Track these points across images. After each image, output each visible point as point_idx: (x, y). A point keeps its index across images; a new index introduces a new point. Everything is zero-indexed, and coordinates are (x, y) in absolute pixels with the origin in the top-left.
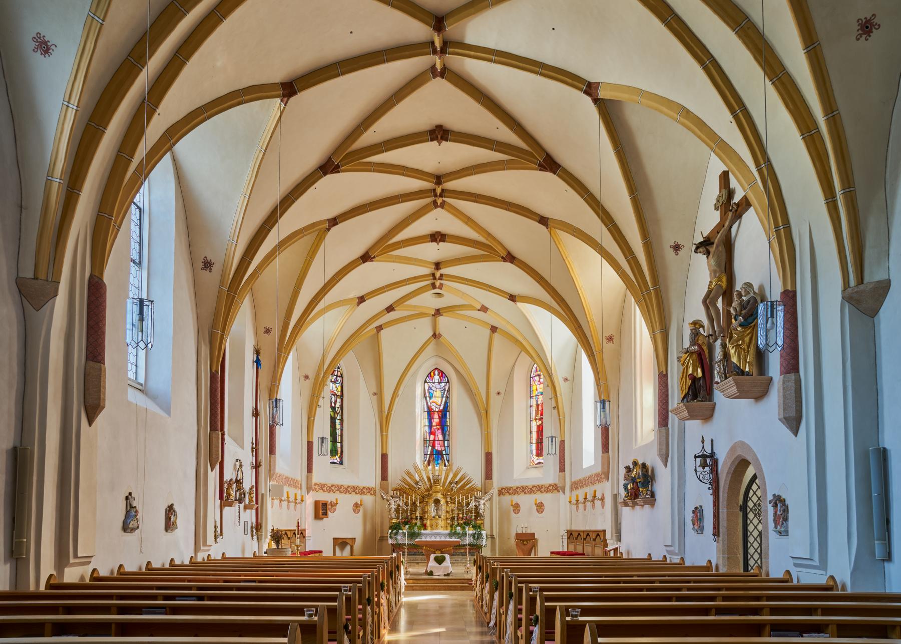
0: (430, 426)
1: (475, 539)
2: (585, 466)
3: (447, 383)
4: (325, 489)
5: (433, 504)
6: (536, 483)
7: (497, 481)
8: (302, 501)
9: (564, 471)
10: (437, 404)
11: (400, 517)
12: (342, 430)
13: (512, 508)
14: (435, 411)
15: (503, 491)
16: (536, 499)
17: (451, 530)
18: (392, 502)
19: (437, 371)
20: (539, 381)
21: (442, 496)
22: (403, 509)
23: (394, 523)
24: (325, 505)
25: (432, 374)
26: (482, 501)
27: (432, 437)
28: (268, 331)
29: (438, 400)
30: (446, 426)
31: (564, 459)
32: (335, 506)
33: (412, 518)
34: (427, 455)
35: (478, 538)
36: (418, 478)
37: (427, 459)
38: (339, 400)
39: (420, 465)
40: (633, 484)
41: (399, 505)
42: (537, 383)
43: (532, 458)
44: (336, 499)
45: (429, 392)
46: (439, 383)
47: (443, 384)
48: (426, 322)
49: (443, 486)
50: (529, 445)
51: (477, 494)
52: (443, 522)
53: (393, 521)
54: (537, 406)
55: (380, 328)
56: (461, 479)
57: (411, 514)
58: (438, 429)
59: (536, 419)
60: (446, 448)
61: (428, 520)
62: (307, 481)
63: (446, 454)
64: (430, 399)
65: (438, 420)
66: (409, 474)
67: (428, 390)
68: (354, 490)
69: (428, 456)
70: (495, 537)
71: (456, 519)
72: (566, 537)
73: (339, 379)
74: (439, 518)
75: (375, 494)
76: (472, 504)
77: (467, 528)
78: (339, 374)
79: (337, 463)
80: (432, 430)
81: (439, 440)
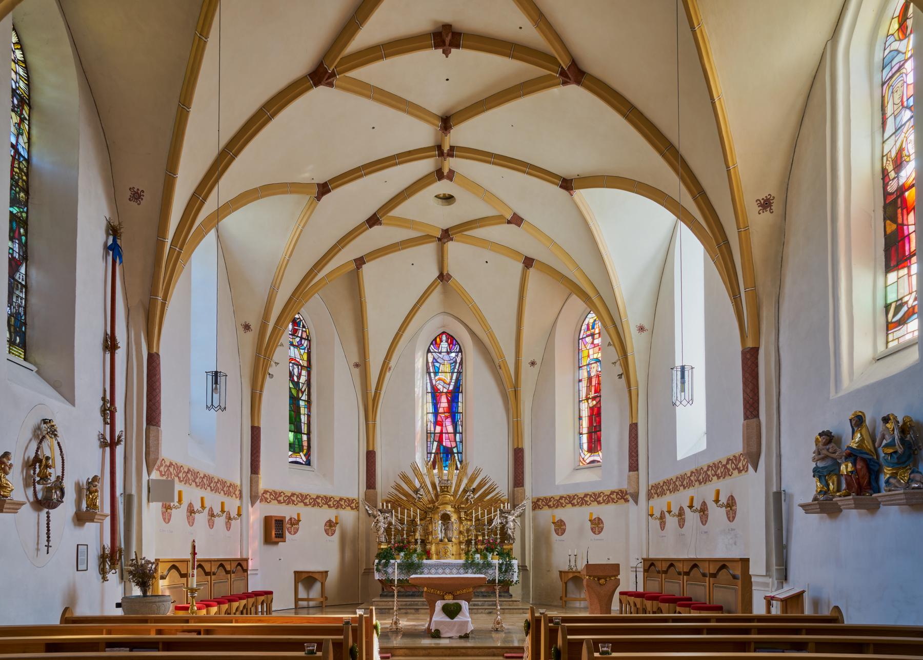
0: (436, 413)
1: (502, 573)
2: (682, 453)
3: (458, 352)
4: (331, 503)
5: (440, 522)
6: (590, 491)
7: (530, 490)
8: (239, 515)
9: (637, 470)
10: (445, 383)
11: (393, 541)
12: (309, 416)
13: (553, 526)
14: (442, 392)
15: (540, 503)
16: (591, 514)
17: (467, 559)
18: (381, 518)
19: (444, 336)
20: (592, 343)
21: (453, 510)
22: (396, 529)
23: (382, 549)
24: (280, 522)
25: (438, 340)
26: (510, 517)
27: (438, 429)
28: (137, 196)
29: (447, 377)
30: (458, 413)
31: (637, 451)
32: (298, 524)
33: (409, 542)
35: (506, 571)
36: (417, 485)
37: (432, 459)
38: (304, 373)
39: (423, 469)
40: (854, 464)
42: (589, 346)
43: (582, 454)
44: (298, 515)
45: (434, 366)
46: (448, 353)
47: (453, 355)
48: (430, 249)
49: (454, 495)
50: (577, 437)
51: (504, 507)
52: (455, 546)
53: (382, 547)
54: (590, 379)
55: (360, 262)
56: (480, 486)
57: (408, 535)
58: (447, 418)
59: (587, 399)
60: (458, 443)
61: (432, 544)
62: (251, 486)
63: (458, 453)
64: (435, 376)
66: (405, 478)
68: (327, 501)
69: (433, 455)
70: (528, 569)
71: (473, 544)
72: (642, 570)
73: (305, 343)
74: (449, 541)
75: (357, 508)
76: (497, 521)
77: (490, 556)
78: (304, 336)
80: (439, 419)
81: (448, 433)
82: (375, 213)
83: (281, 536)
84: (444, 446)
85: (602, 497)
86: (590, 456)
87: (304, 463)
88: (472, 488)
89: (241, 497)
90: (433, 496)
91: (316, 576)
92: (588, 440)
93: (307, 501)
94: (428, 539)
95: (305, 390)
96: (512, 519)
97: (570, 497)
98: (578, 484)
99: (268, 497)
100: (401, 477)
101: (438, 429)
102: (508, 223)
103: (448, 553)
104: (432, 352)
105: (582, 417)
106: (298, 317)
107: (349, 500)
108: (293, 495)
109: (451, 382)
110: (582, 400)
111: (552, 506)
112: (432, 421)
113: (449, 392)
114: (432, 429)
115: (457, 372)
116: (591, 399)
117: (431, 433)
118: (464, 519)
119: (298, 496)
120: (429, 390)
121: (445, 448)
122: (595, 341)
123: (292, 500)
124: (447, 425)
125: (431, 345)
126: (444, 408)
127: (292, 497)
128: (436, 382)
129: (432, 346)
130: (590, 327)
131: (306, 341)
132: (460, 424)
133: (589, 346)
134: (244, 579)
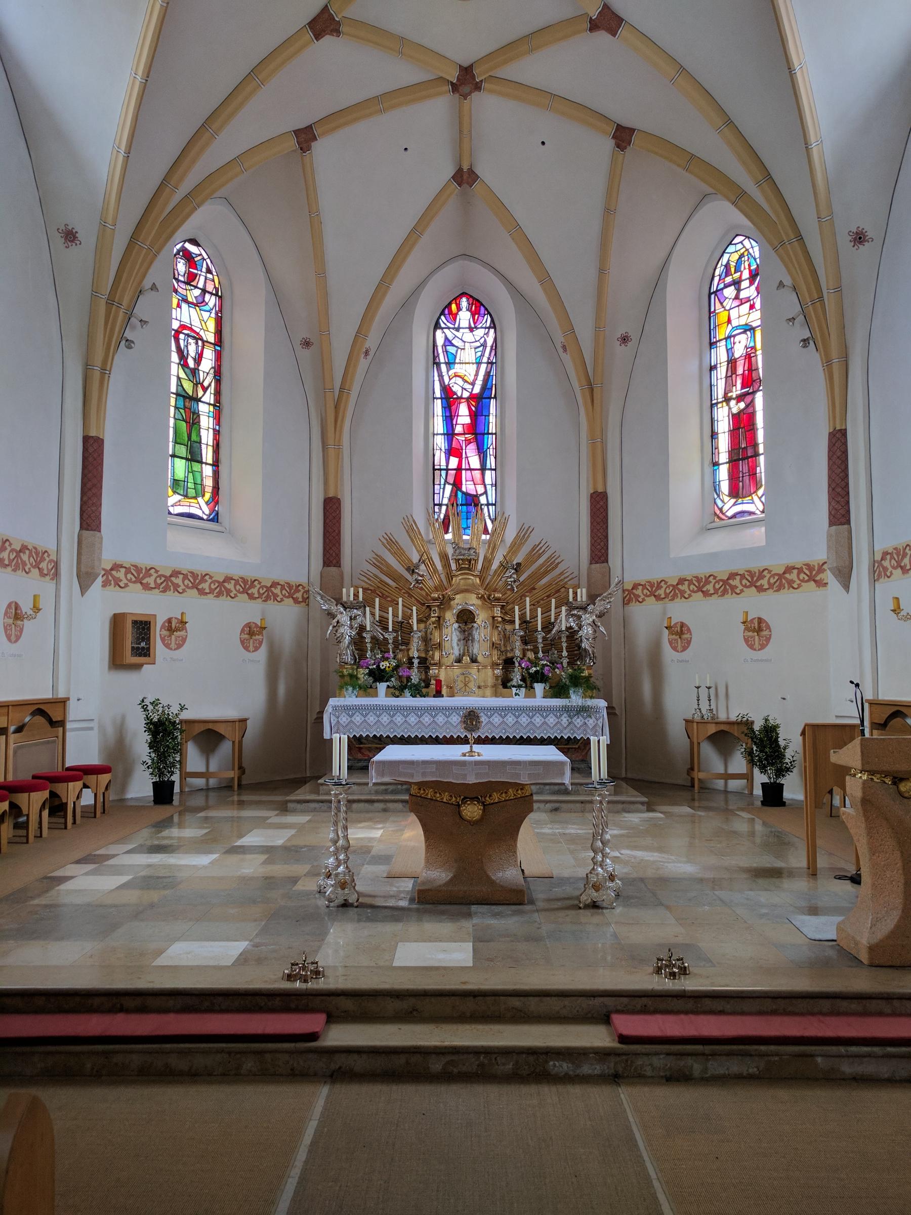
3: (489, 328)
4: (254, 591)
6: (740, 566)
9: (848, 522)
10: (466, 381)
14: (461, 398)
15: (639, 592)
18: (344, 618)
19: (464, 300)
21: (479, 602)
22: (374, 638)
24: (143, 627)
25: (454, 307)
27: (454, 462)
29: (469, 371)
30: (488, 434)
31: (847, 484)
34: (440, 505)
36: (415, 558)
38: (209, 354)
41: (362, 628)
45: (447, 352)
46: (471, 330)
47: (480, 333)
50: (708, 469)
56: (534, 554)
58: (468, 442)
60: (489, 487)
65: (467, 420)
66: (391, 544)
67: (444, 345)
75: (306, 600)
79: (204, 520)
80: (454, 445)
82: (326, 6)
83: (144, 651)
84: (463, 493)
85: (766, 579)
86: (734, 504)
87: (205, 517)
88: (515, 563)
89: (56, 575)
90: (443, 577)
91: (221, 729)
92: (729, 476)
93: (206, 586)
94: (433, 659)
95: (210, 385)
96: (591, 620)
97: (698, 579)
98: (714, 555)
99: (181, 583)
100: (385, 542)
101: (454, 462)
102: (591, 29)
103: (472, 685)
104: (443, 329)
105: (717, 434)
106: (198, 252)
107: (290, 586)
108: (176, 573)
109: (475, 379)
110: (717, 404)
111: (663, 596)
112: (443, 449)
113: (472, 397)
114: (443, 463)
115: (488, 363)
116: (734, 399)
117: (440, 470)
118: (500, 619)
119: (185, 577)
120: (438, 394)
121: (466, 494)
122: (742, 293)
123: (273, 593)
124: (468, 456)
125: (441, 315)
126: (463, 425)
127: (273, 589)
128: (450, 379)
129: (443, 317)
130: (733, 270)
131: (213, 298)
132: (491, 453)
133: (728, 304)
134: (54, 742)
